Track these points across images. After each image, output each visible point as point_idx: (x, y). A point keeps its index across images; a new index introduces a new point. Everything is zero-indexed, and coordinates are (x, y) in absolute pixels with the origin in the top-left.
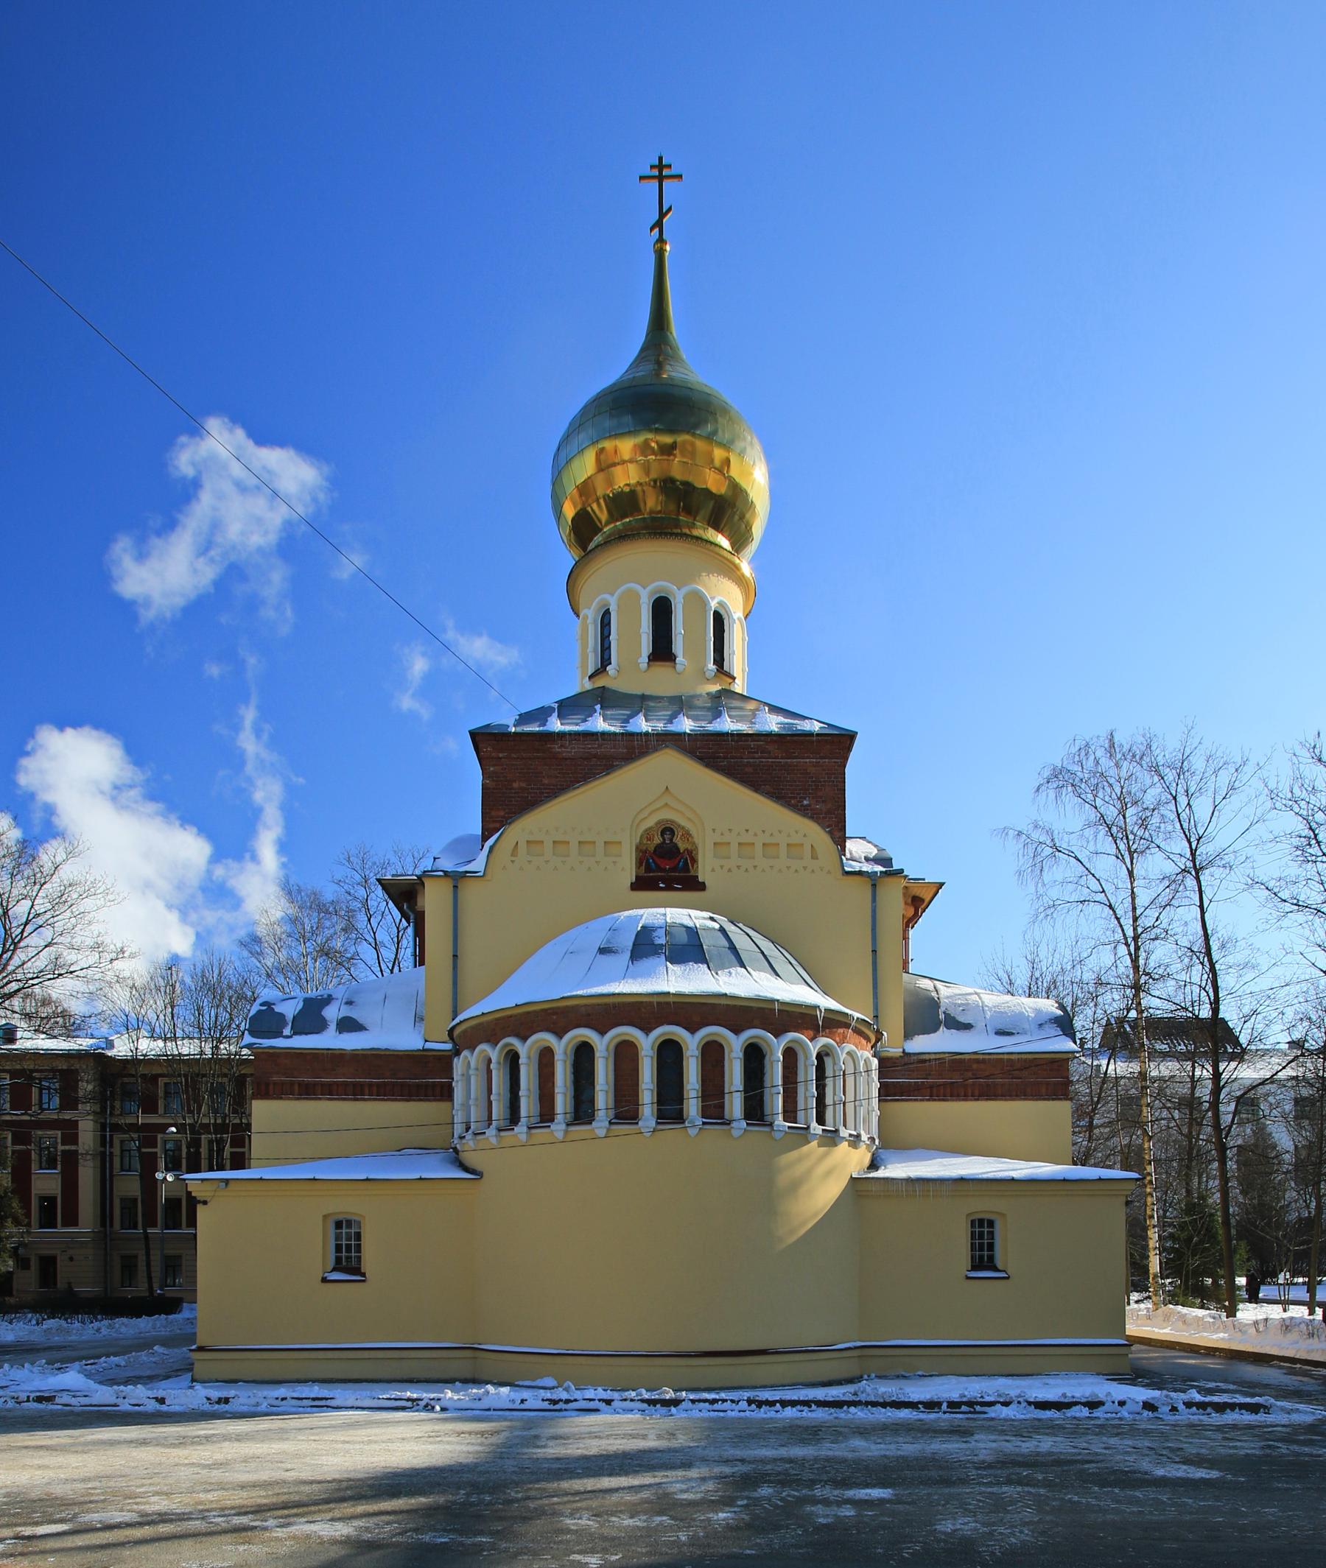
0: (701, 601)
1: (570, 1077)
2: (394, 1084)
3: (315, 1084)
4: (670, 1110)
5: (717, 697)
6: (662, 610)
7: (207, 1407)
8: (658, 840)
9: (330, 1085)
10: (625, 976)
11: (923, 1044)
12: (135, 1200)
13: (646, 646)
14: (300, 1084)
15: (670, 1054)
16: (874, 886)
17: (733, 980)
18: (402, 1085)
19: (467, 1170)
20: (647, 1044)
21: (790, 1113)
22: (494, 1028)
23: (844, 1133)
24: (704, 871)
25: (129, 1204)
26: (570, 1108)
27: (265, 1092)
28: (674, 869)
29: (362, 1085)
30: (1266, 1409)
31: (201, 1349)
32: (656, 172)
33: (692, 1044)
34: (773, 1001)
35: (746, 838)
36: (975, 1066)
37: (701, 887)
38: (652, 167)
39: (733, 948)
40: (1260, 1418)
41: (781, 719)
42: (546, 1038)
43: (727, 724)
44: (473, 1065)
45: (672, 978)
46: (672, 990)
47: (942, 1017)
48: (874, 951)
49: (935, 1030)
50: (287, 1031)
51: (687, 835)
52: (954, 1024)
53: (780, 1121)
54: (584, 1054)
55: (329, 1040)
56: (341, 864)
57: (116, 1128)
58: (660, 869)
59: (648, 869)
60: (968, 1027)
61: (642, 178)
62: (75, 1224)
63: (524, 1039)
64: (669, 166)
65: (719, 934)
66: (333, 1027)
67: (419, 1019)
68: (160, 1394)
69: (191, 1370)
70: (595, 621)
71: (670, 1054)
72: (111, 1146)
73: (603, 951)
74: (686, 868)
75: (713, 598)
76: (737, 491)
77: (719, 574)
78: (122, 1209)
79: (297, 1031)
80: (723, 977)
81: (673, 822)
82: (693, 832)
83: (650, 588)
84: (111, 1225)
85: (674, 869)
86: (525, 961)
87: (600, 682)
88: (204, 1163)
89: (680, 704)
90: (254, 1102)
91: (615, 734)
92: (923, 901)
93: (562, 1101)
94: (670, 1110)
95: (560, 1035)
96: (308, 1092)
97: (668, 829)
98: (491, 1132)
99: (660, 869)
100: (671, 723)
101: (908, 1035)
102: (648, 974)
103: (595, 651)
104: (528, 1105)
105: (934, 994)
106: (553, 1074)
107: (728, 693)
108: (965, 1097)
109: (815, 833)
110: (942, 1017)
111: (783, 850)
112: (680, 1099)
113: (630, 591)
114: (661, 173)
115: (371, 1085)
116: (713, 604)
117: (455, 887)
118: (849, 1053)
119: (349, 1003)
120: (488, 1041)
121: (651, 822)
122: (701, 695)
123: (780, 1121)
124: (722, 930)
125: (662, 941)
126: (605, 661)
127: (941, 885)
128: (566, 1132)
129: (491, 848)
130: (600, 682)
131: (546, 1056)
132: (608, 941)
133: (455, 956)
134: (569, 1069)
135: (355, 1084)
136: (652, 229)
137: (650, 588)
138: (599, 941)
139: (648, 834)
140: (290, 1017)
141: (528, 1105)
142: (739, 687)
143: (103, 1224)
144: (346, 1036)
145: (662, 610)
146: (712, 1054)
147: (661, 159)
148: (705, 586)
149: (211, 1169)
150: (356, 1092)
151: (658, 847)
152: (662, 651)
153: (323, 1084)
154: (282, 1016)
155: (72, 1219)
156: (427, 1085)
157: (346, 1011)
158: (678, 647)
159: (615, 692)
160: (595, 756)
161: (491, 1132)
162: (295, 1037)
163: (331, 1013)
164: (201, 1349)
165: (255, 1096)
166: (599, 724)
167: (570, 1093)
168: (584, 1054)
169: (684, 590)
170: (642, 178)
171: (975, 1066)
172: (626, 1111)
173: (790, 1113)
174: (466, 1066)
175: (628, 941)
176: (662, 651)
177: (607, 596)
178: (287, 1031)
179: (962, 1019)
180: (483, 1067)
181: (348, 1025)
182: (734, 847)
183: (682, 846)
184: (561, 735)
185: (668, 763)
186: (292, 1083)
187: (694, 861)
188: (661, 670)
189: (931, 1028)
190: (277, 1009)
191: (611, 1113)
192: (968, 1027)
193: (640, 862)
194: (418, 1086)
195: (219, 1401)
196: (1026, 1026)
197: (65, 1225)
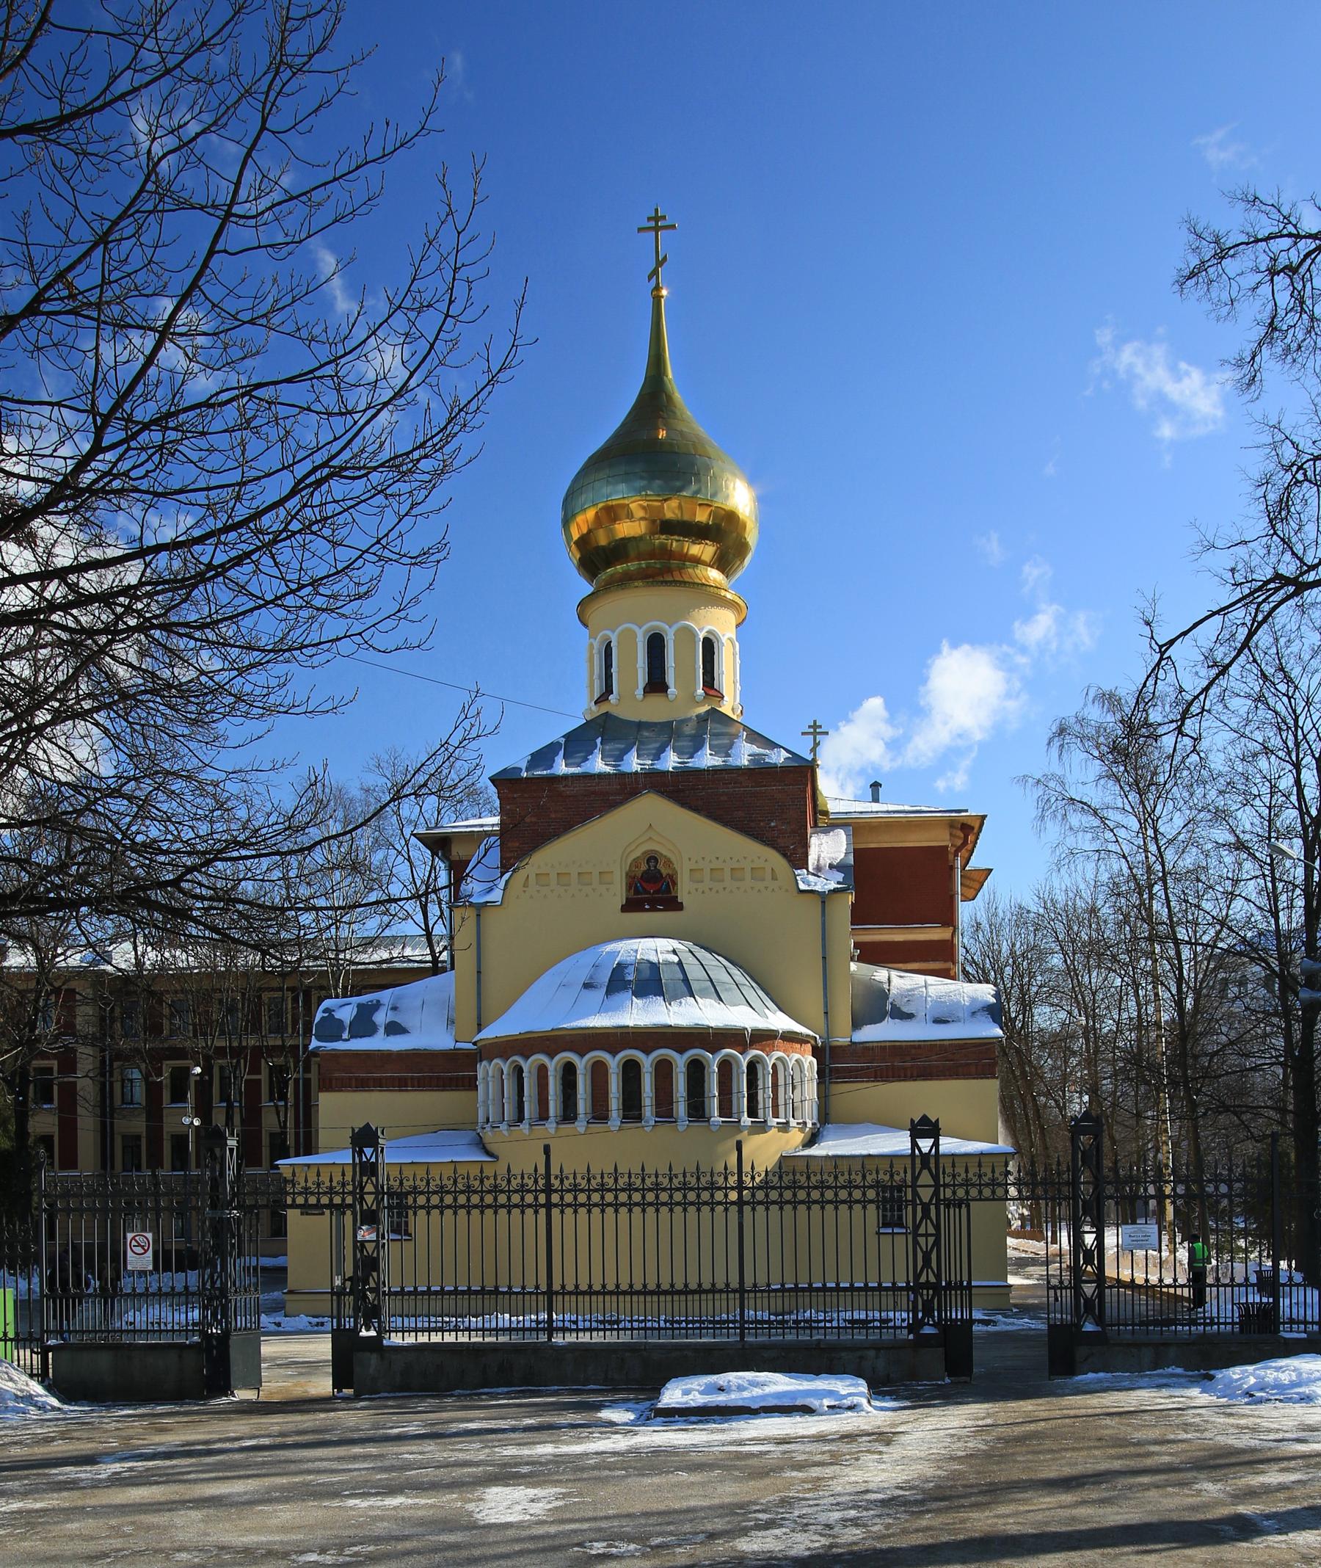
0: (691, 633)
1: (559, 1087)
2: (431, 1077)
3: (368, 1078)
4: (632, 1109)
5: (702, 719)
6: (656, 644)
7: (309, 1328)
8: (644, 867)
9: (380, 1079)
10: (601, 1010)
11: (870, 1033)
12: (138, 1137)
13: (642, 678)
14: (357, 1078)
15: (631, 1070)
16: (823, 902)
17: (682, 1009)
18: (438, 1078)
19: (489, 1153)
20: (614, 1064)
21: (726, 1110)
22: (505, 1048)
23: (773, 1121)
24: (684, 891)
25: (132, 1143)
26: (560, 1112)
27: (328, 1086)
28: (658, 892)
29: (405, 1079)
30: (995, 1323)
31: (291, 1292)
32: (652, 224)
33: (647, 1062)
34: (709, 1027)
35: (715, 865)
36: (913, 1051)
37: (678, 906)
38: (649, 219)
39: (686, 980)
40: (990, 1328)
41: (755, 749)
42: (542, 1058)
43: (707, 759)
44: (490, 1073)
45: (635, 1011)
46: (631, 1024)
47: (889, 1007)
48: (824, 958)
49: (881, 1020)
50: (345, 1036)
51: (669, 862)
52: (900, 1014)
53: (716, 1118)
54: (569, 1070)
55: (378, 1042)
56: (370, 771)
57: (119, 1056)
58: (646, 892)
59: (637, 892)
60: (910, 1016)
61: (640, 230)
62: (74, 1165)
63: (527, 1057)
64: (664, 218)
65: (677, 968)
66: (382, 1030)
67: (451, 1022)
68: (278, 1320)
69: (283, 1308)
70: (600, 652)
71: (631, 1070)
72: (111, 1076)
73: (587, 986)
74: (669, 891)
75: (701, 630)
76: (731, 517)
77: (706, 606)
78: (124, 1148)
79: (353, 1035)
80: (675, 1007)
81: (656, 852)
82: (673, 859)
83: (645, 627)
84: (112, 1167)
85: (658, 892)
86: (528, 985)
87: (604, 708)
88: (292, 1151)
89: (667, 733)
90: (321, 1095)
91: (609, 774)
92: (973, 828)
93: (554, 1107)
94: (632, 1109)
95: (552, 1056)
96: (363, 1085)
97: (652, 858)
98: (503, 1127)
99: (646, 892)
100: (659, 759)
101: (856, 1025)
102: (616, 1009)
103: (600, 677)
104: (530, 1109)
105: (886, 986)
106: (547, 1084)
107: (715, 715)
108: (913, 1078)
109: (773, 859)
110: (889, 1007)
111: (748, 874)
112: (639, 1106)
113: (628, 630)
114: (657, 224)
115: (412, 1078)
116: (701, 636)
117: (478, 915)
118: (778, 1059)
119: (394, 1009)
120: (501, 1057)
121: (638, 853)
122: (690, 719)
123: (716, 1118)
124: (680, 964)
125: (631, 977)
126: (609, 690)
127: (984, 817)
128: (557, 1129)
129: (507, 882)
130: (604, 708)
131: (542, 1071)
132: (591, 978)
133: (479, 972)
134: (559, 1082)
135: (400, 1079)
136: (665, 258)
137: (645, 627)
138: (583, 978)
139: (636, 862)
140: (347, 1022)
141: (530, 1109)
142: (726, 708)
143: (104, 1166)
144: (392, 1038)
145: (656, 644)
146: (664, 1070)
147: (656, 210)
148: (697, 623)
149: (297, 1155)
150: (401, 1084)
151: (645, 872)
152: (656, 684)
153: (374, 1079)
154: (340, 1021)
155: (70, 1160)
156: (457, 1078)
157: (391, 1017)
158: (670, 678)
159: (616, 718)
160: (594, 793)
161: (503, 1127)
162: (353, 1041)
163: (381, 1018)
164: (291, 1292)
165: (321, 1090)
166: (598, 765)
167: (560, 1099)
168: (569, 1070)
169: (675, 627)
170: (640, 230)
171: (913, 1051)
172: (600, 1113)
173: (726, 1110)
174: (485, 1070)
175: (605, 977)
176: (656, 684)
177: (608, 633)
178: (345, 1036)
179: (905, 1009)
180: (497, 1075)
181: (394, 1029)
182: (707, 872)
183: (664, 872)
184: (565, 777)
185: (650, 806)
186: (350, 1078)
187: (675, 883)
188: (656, 699)
189: (877, 1019)
190: (337, 1015)
191: (589, 1116)
192: (910, 1016)
193: (629, 887)
194: (451, 1079)
195: (317, 1324)
196: (961, 1015)
197: (62, 1167)
